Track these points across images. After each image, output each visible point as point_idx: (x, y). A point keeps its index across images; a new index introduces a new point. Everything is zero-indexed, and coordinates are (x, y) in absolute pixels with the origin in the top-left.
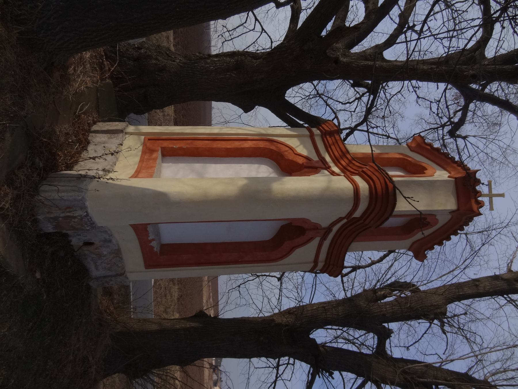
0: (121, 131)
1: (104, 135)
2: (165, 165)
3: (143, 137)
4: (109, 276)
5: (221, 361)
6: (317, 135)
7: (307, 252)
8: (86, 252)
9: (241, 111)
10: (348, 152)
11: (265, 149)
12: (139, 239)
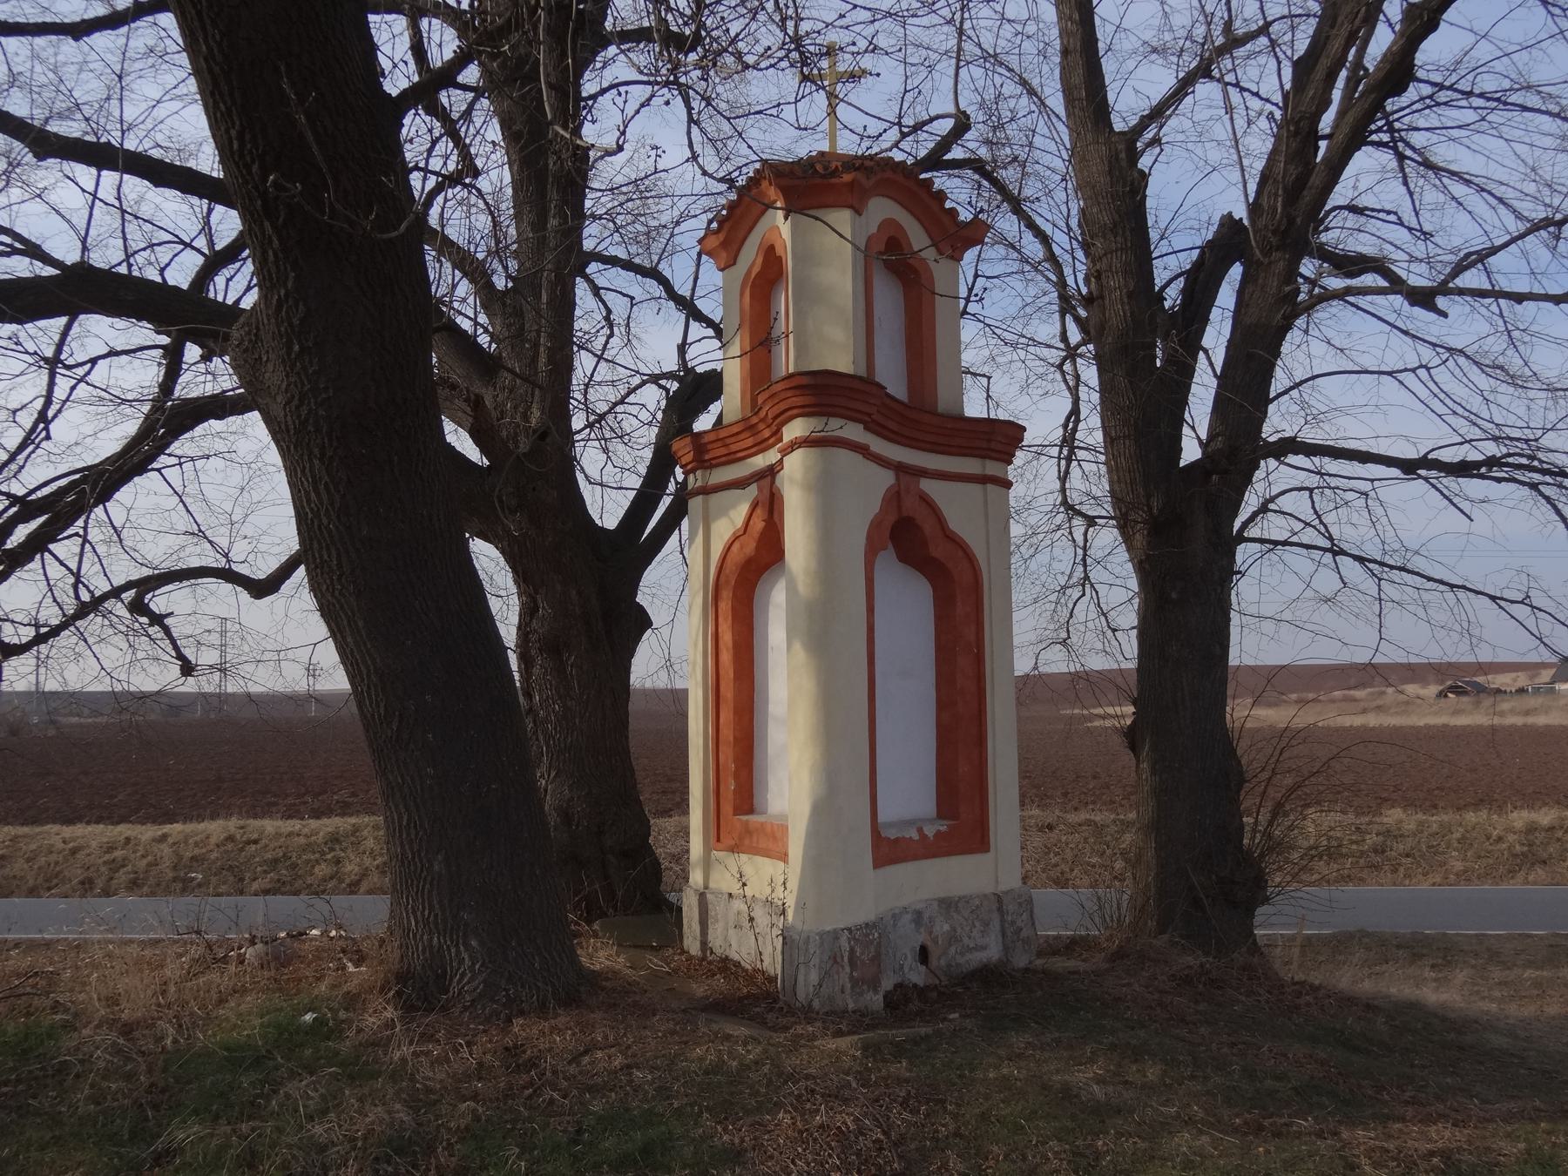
0: (702, 896)
4: (1002, 927)
7: (957, 506)
8: (943, 962)
10: (744, 420)
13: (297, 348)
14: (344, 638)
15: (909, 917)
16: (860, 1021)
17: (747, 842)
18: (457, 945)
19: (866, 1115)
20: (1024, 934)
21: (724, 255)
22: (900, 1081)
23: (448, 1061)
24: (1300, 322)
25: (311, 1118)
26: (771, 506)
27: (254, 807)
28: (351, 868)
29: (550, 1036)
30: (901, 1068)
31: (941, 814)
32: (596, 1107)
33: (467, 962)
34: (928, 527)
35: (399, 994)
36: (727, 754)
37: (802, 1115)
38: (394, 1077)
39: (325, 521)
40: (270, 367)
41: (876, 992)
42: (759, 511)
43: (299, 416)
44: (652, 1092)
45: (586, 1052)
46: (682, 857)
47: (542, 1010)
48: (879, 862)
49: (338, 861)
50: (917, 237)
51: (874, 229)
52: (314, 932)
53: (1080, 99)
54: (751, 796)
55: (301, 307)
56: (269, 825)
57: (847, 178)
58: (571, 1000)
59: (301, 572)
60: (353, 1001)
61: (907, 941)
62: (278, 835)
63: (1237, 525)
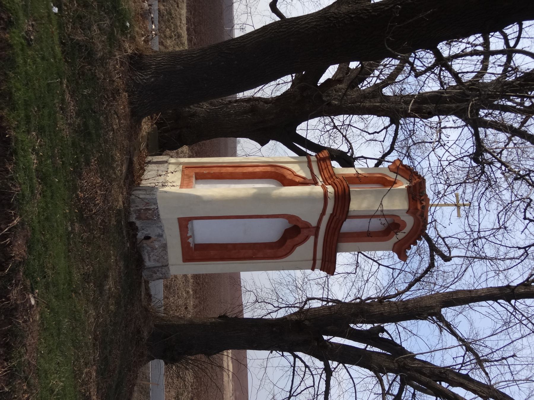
0: (166, 162)
1: (154, 165)
2: (197, 185)
3: (181, 166)
4: (157, 267)
6: (314, 161)
7: (305, 250)
8: (145, 245)
9: (258, 145)
10: (334, 174)
11: (271, 172)
13: (353, 16)
14: (256, 34)
15: (161, 233)
16: (127, 212)
17: (186, 177)
18: (152, 74)
19: (100, 208)
20: (154, 275)
21: (394, 167)
22: (110, 220)
23: (115, 70)
24: (372, 373)
25: (98, 25)
26: (304, 183)
27: (190, 6)
28: (169, 42)
29: (122, 105)
30: (114, 222)
31: (196, 245)
32: (101, 118)
33: (146, 77)
34: (297, 239)
35: (135, 54)
36: (216, 170)
37: (100, 186)
38: (110, 52)
39: (295, 27)
40: (347, 7)
41: (136, 218)
42: (302, 180)
43: (330, 17)
44: (106, 137)
45: (118, 116)
46: (178, 156)
47: (130, 103)
49: (171, 37)
50: (401, 236)
51: (402, 218)
52: (153, 26)
53: (453, 296)
54: (201, 179)
55: (366, 17)
56: (184, 12)
57: (419, 206)
58: (133, 113)
59: (278, 19)
60: (133, 38)
61: (153, 232)
62: (180, 15)
63: (300, 354)
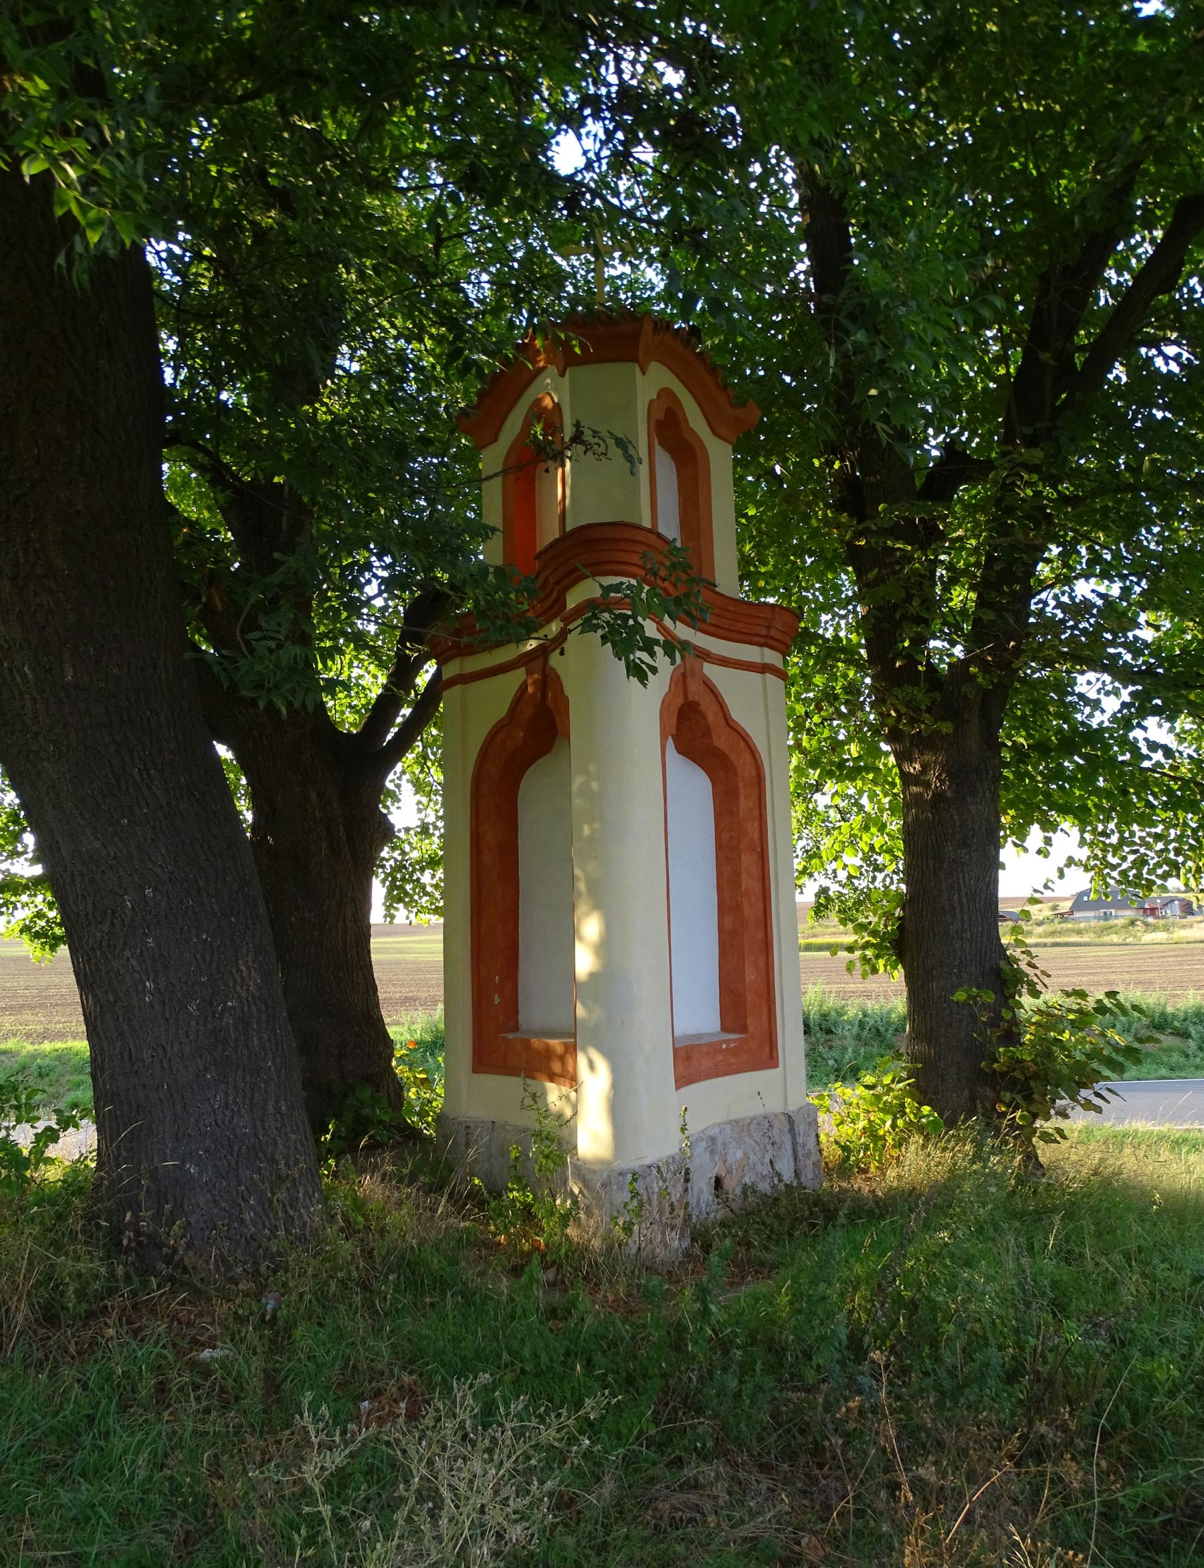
5: (381, 665)
12: (708, 1077)
15: (704, 1144)
31: (724, 1028)
34: (712, 715)
48: (683, 1080)
